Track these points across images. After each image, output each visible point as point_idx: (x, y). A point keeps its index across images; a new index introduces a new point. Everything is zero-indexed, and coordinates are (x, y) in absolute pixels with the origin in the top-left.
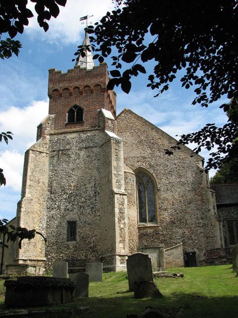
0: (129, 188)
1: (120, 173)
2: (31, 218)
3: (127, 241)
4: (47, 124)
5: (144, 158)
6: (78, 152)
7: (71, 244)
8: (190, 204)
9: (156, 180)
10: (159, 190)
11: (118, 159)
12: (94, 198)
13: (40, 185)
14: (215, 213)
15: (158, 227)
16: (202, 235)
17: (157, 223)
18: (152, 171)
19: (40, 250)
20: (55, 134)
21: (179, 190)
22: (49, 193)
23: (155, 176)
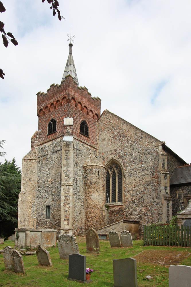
0: (94, 178)
1: (68, 169)
2: (25, 205)
3: (71, 219)
4: (35, 138)
5: (116, 150)
6: (51, 155)
7: (48, 220)
8: (147, 186)
9: (123, 167)
10: (125, 176)
11: (68, 158)
12: (59, 189)
14: (167, 193)
15: (123, 205)
16: (156, 212)
17: (122, 203)
18: (120, 161)
19: (32, 225)
20: (40, 145)
21: (140, 175)
22: (37, 187)
23: (123, 165)
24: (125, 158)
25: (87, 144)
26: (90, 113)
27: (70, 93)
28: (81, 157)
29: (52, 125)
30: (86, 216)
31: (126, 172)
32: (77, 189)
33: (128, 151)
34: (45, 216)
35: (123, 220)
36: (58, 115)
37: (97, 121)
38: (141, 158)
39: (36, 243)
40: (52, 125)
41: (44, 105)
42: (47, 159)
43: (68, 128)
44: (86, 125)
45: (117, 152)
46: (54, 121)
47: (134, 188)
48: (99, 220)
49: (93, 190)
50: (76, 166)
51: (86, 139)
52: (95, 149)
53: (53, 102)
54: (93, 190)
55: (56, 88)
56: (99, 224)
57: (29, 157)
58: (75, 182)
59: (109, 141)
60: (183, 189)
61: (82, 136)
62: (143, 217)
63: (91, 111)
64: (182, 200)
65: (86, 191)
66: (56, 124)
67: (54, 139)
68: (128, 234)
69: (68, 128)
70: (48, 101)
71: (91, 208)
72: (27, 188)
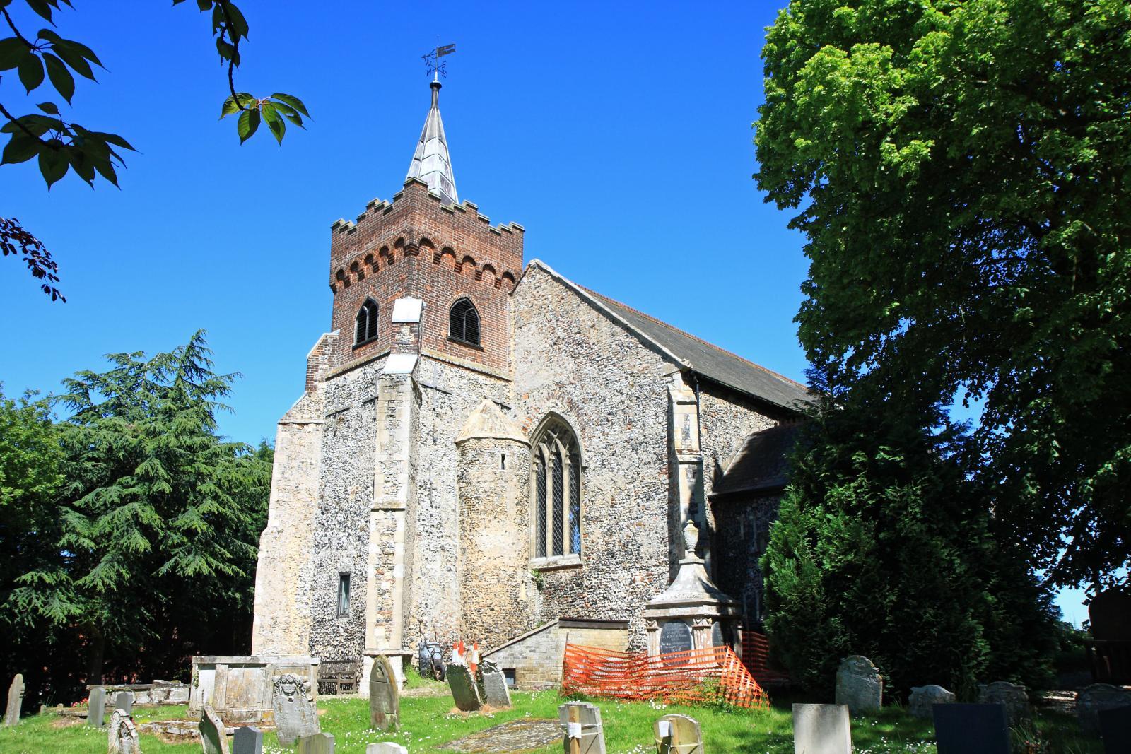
0: (486, 478)
1: (396, 457)
4: (320, 357)
5: (561, 386)
6: (360, 411)
8: (648, 500)
10: (586, 467)
13: (300, 496)
15: (580, 566)
19: (299, 639)
21: (626, 464)
22: (319, 511)
24: (585, 409)
25: (473, 371)
26: (487, 273)
27: (416, 227)
28: (449, 412)
29: (368, 317)
30: (464, 606)
31: (589, 454)
32: (431, 516)
33: (593, 387)
34: (335, 608)
35: (557, 620)
36: (384, 288)
37: (511, 294)
38: (627, 410)
39: (247, 702)
40: (368, 317)
41: (349, 258)
42: (348, 421)
43: (402, 330)
44: (473, 310)
45: (563, 390)
46: (372, 306)
47: (612, 506)
48: (504, 618)
49: (485, 517)
50: (430, 442)
51: (470, 355)
52: (502, 383)
53: (371, 251)
54: (485, 517)
55: (381, 212)
56: (504, 631)
57: (299, 417)
58: (426, 493)
59: (544, 356)
60: (757, 509)
61: (457, 346)
62: (638, 604)
63: (488, 267)
64: (755, 544)
65: (462, 522)
66: (377, 316)
67: (369, 362)
68: (494, 670)
69: (402, 330)
70: (360, 248)
71: (477, 577)
72: (287, 516)
